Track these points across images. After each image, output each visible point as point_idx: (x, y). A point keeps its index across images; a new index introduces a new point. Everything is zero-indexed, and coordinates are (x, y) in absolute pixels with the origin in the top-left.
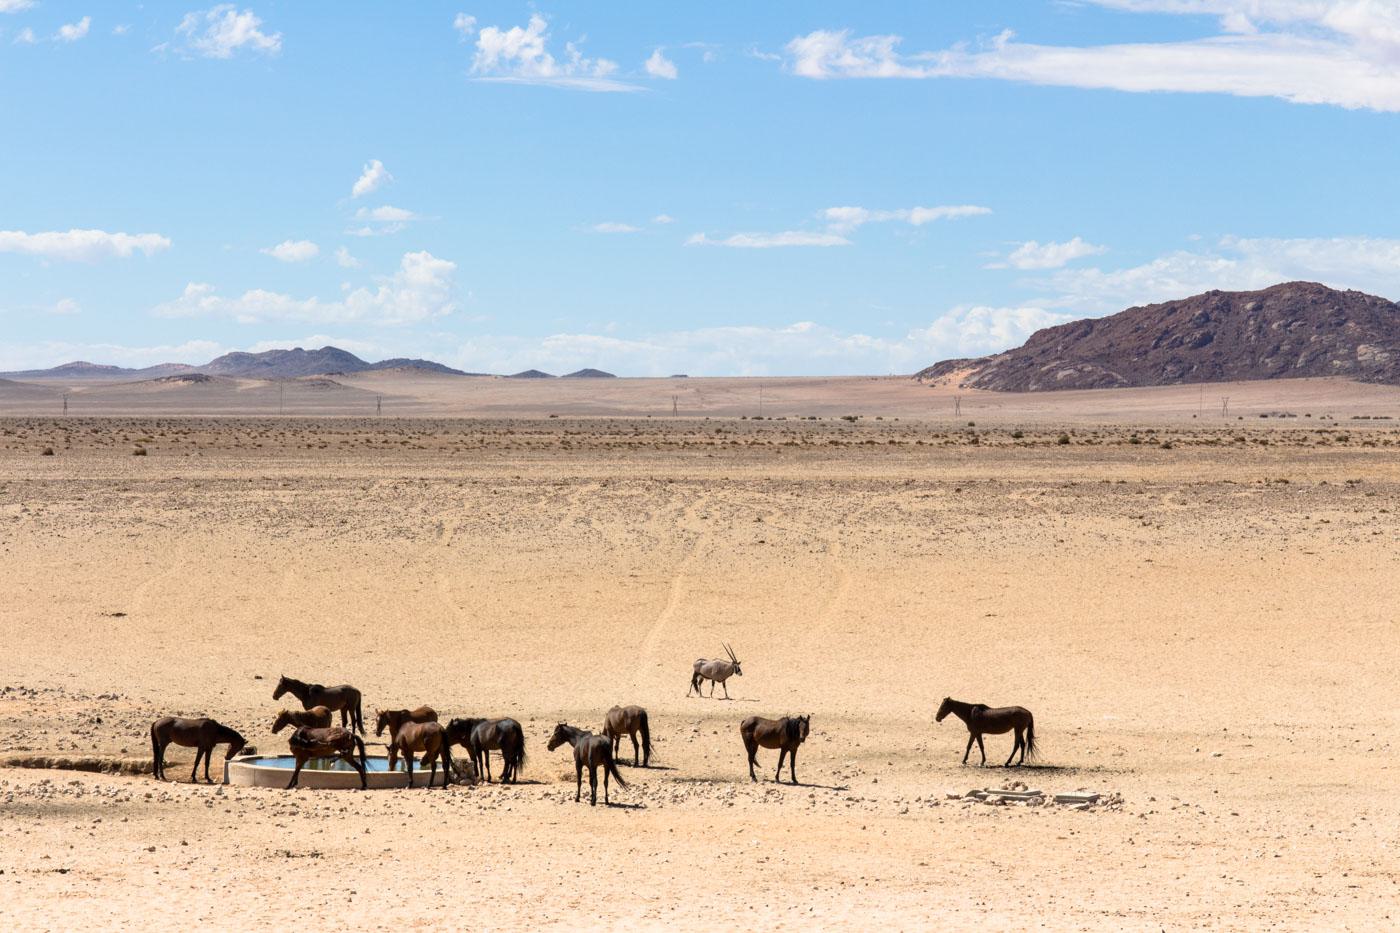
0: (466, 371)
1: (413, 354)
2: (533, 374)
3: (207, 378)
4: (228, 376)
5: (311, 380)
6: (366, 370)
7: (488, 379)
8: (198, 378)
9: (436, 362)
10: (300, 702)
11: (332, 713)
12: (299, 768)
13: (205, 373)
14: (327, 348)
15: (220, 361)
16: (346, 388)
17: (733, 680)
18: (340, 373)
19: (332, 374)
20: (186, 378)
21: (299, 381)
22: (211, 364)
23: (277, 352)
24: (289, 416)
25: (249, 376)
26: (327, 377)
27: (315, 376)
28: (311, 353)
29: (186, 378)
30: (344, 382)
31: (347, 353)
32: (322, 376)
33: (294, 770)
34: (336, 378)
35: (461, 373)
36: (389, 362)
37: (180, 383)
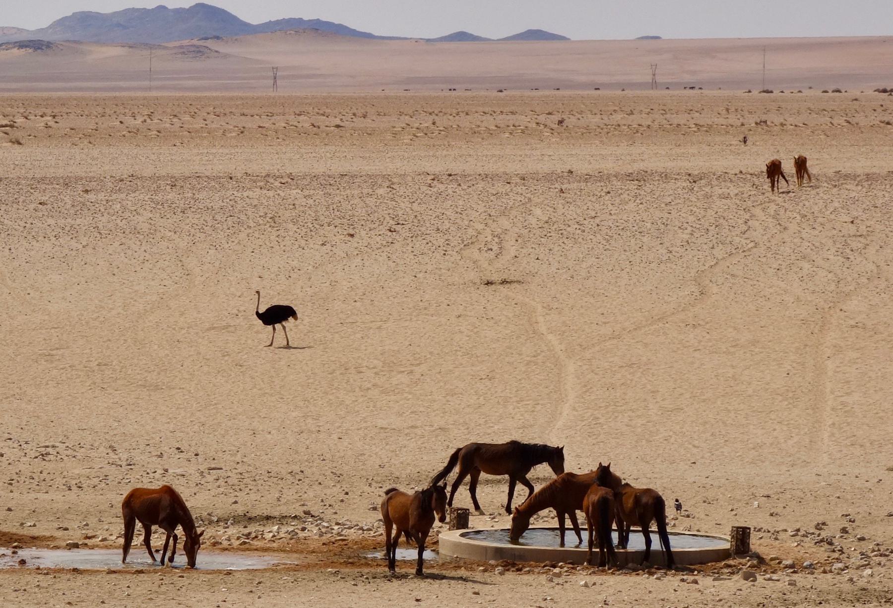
0: (376, 33)
1: (308, 15)
2: (462, 36)
3: (49, 45)
4: (75, 42)
5: (181, 47)
6: (546, 39)
7: (557, 44)
8: (36, 45)
9: (336, 23)
10: (550, 470)
11: (566, 471)
12: (420, 554)
13: (46, 38)
14: (197, 5)
15: (62, 22)
16: (226, 56)
17: (290, 323)
18: (218, 38)
19: (206, 39)
20: (22, 45)
21: (165, 48)
22: (50, 27)
23: (134, 10)
24: (193, 94)
25: (98, 43)
26: (201, 43)
27: (186, 42)
28: (179, 11)
29: (22, 45)
30: (223, 48)
31: (224, 11)
32: (195, 42)
33: (417, 557)
34: (209, 43)
35: (368, 36)
36: (278, 22)
37: (15, 51)
